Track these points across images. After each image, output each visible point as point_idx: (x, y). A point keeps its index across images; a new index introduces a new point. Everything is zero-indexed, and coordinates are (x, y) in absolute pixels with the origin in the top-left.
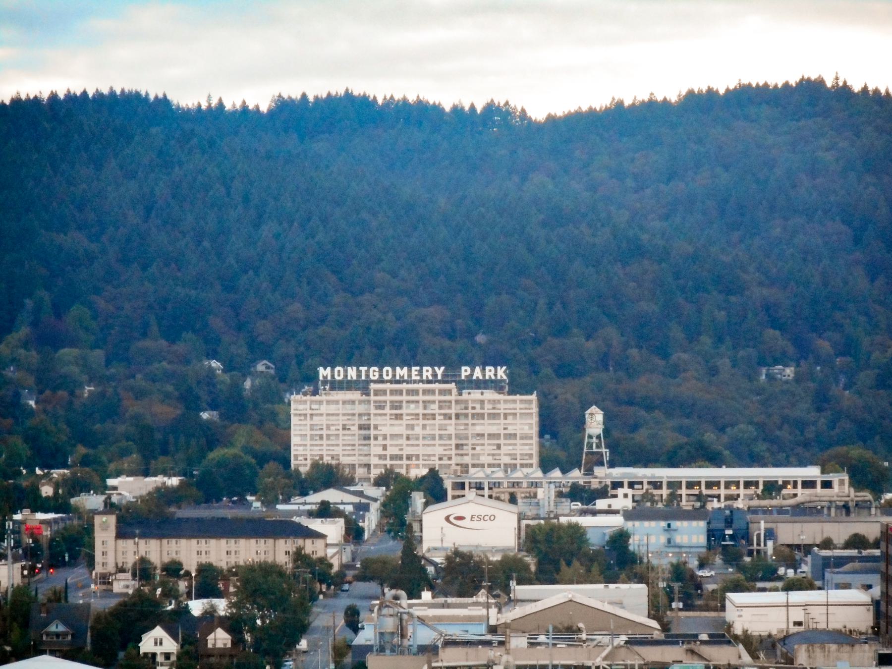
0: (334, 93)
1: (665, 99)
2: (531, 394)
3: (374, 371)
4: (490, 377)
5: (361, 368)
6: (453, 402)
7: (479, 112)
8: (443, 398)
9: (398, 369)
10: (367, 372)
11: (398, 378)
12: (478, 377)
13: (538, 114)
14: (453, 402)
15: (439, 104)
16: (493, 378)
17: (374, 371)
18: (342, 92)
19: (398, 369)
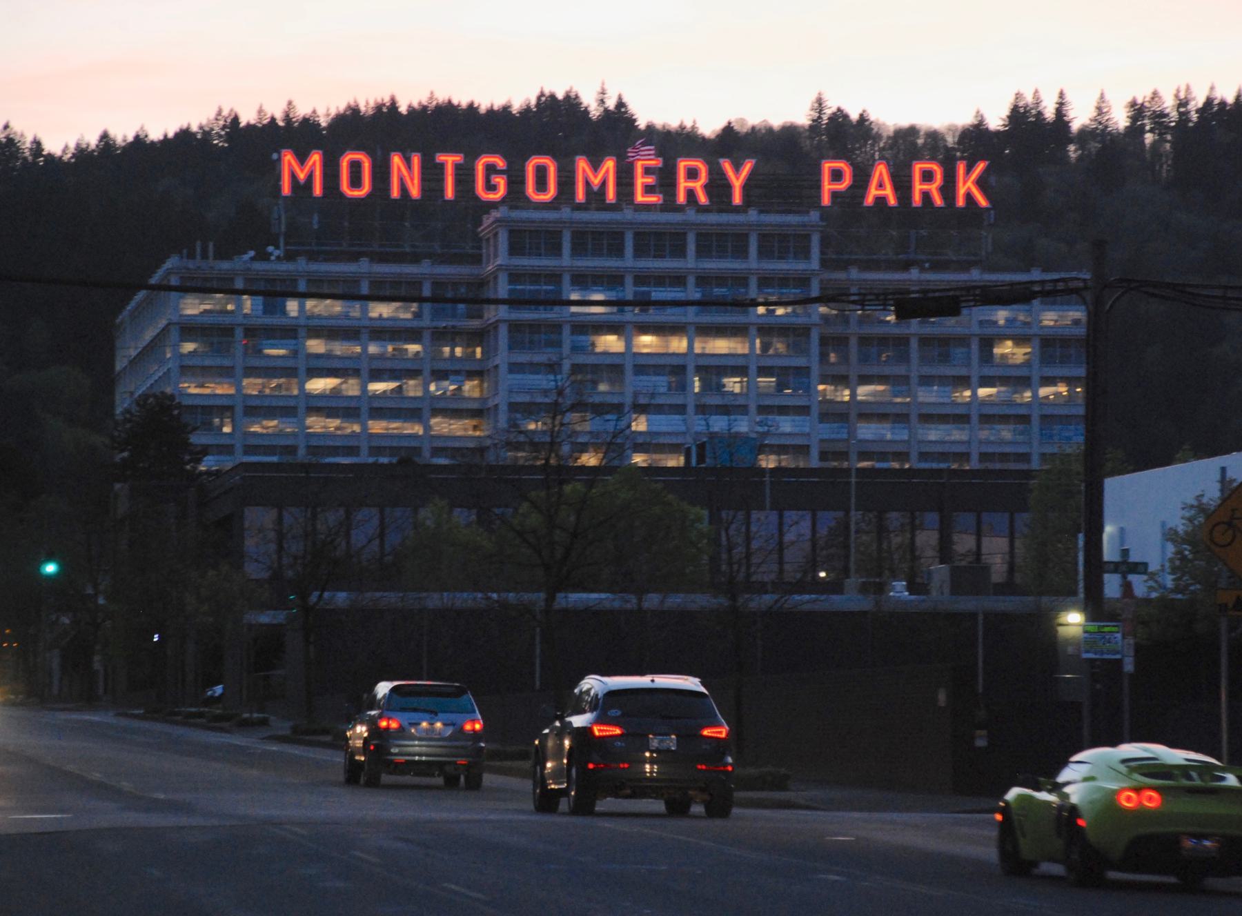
0: (415, 105)
1: (105, 136)
2: (442, 166)
3: (491, 169)
4: (926, 196)
5: (441, 158)
6: (914, 344)
7: (242, 125)
8: (712, 265)
9: (582, 164)
10: (464, 176)
11: (580, 196)
12: (881, 200)
13: (57, 143)
14: (914, 344)
15: (577, 97)
16: (938, 201)
17: (491, 169)
18: (92, 140)
19: (582, 164)
